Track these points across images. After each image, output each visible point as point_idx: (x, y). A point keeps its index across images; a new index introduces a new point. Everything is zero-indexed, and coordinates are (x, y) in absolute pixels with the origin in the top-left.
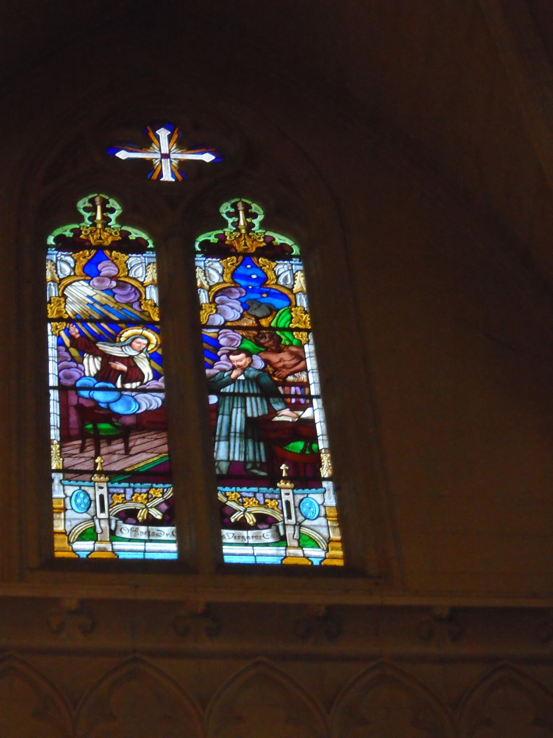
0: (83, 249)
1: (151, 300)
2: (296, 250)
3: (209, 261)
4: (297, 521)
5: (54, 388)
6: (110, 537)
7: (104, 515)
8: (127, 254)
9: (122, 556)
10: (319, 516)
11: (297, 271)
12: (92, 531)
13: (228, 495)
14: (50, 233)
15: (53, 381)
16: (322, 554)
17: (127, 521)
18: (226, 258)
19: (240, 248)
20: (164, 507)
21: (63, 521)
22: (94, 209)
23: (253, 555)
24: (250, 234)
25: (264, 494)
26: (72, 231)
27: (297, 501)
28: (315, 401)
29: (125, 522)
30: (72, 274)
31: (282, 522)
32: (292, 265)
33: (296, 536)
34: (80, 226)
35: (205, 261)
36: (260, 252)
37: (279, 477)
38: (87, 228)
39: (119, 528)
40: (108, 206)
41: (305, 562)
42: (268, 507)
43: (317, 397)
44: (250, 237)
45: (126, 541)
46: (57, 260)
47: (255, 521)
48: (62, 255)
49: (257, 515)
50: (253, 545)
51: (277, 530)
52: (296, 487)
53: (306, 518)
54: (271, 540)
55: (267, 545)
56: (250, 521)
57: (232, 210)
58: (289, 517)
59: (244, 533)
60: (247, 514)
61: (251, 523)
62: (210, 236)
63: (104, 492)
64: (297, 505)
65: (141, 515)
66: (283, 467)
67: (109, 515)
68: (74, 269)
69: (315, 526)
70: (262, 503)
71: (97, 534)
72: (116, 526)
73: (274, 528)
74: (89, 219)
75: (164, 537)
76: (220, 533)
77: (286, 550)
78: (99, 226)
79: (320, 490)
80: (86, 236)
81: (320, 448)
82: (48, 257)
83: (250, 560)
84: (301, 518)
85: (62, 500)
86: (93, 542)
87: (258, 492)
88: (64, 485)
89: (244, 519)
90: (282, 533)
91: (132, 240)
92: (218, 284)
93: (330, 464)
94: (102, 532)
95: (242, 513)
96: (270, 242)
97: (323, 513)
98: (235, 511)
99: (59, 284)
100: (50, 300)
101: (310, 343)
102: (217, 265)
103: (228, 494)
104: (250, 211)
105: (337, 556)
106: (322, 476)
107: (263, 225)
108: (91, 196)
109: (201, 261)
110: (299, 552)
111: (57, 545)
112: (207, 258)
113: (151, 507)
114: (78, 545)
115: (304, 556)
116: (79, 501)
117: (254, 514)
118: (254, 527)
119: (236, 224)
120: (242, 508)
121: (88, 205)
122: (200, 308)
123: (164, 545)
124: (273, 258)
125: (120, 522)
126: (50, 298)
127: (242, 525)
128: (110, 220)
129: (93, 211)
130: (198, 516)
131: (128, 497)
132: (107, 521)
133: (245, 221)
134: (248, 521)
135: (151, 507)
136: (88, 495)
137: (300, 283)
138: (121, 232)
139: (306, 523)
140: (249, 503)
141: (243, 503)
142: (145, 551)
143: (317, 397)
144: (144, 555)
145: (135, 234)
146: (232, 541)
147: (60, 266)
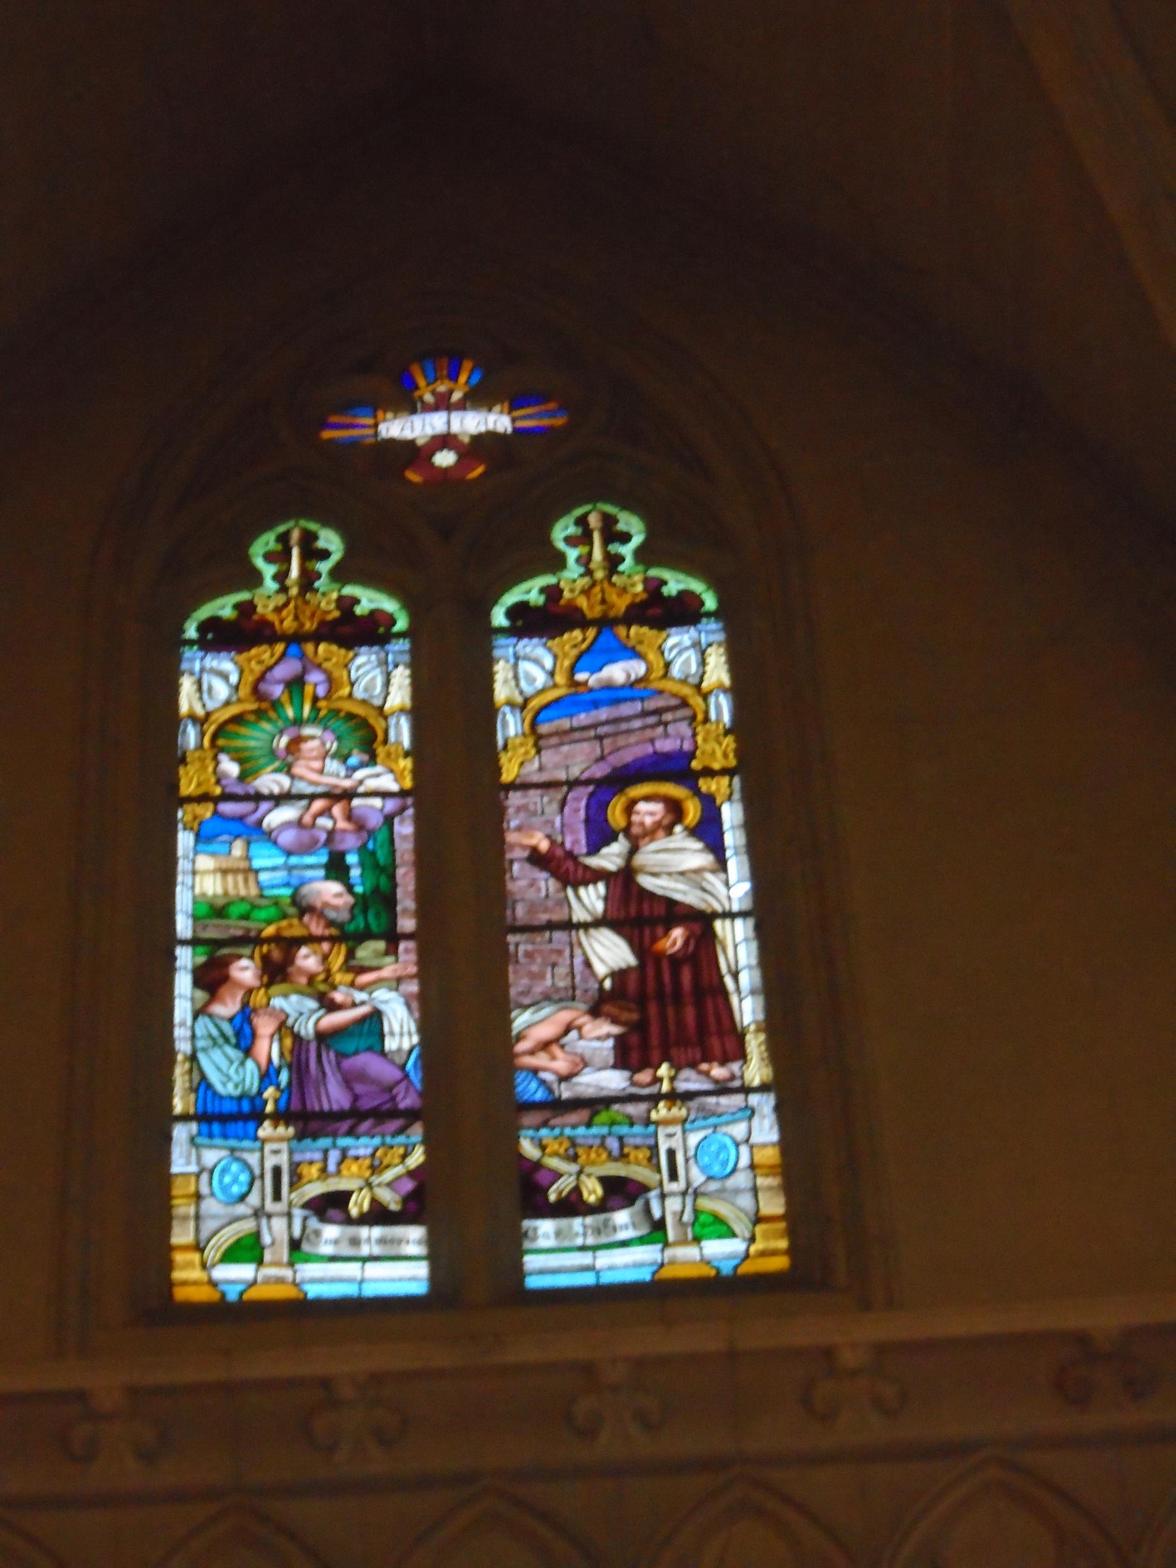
0: (571, 627)
6: (291, 1255)
7: (281, 1207)
9: (313, 1291)
10: (734, 1170)
11: (710, 645)
25: (621, 1139)
26: (542, 590)
30: (234, 698)
32: (700, 632)
49: (605, 1181)
51: (647, 1210)
52: (300, 1136)
55: (624, 1244)
56: (590, 1194)
58: (673, 1176)
59: (577, 1223)
61: (592, 1199)
62: (223, 607)
63: (283, 1160)
65: (358, 1204)
68: (552, 674)
70: (616, 1152)
71: (263, 1249)
72: (304, 1228)
73: (639, 1203)
75: (622, 1235)
77: (663, 1250)
83: (350, 1290)
85: (193, 1179)
86: (659, 1246)
87: (610, 1134)
89: (577, 1190)
90: (657, 1213)
91: (670, 597)
94: (273, 1243)
95: (572, 1178)
96: (654, 587)
97: (744, 1161)
98: (557, 1175)
105: (772, 1252)
107: (641, 555)
108: (281, 529)
113: (379, 1185)
114: (223, 1272)
115: (702, 1260)
116: (227, 1179)
118: (603, 1207)
121: (572, 530)
123: (398, 1268)
125: (314, 1223)
127: (571, 1206)
128: (319, 576)
129: (584, 544)
131: (332, 1167)
135: (379, 1185)
137: (718, 671)
141: (575, 1158)
142: (362, 1282)
145: (675, 583)
146: (550, 1243)
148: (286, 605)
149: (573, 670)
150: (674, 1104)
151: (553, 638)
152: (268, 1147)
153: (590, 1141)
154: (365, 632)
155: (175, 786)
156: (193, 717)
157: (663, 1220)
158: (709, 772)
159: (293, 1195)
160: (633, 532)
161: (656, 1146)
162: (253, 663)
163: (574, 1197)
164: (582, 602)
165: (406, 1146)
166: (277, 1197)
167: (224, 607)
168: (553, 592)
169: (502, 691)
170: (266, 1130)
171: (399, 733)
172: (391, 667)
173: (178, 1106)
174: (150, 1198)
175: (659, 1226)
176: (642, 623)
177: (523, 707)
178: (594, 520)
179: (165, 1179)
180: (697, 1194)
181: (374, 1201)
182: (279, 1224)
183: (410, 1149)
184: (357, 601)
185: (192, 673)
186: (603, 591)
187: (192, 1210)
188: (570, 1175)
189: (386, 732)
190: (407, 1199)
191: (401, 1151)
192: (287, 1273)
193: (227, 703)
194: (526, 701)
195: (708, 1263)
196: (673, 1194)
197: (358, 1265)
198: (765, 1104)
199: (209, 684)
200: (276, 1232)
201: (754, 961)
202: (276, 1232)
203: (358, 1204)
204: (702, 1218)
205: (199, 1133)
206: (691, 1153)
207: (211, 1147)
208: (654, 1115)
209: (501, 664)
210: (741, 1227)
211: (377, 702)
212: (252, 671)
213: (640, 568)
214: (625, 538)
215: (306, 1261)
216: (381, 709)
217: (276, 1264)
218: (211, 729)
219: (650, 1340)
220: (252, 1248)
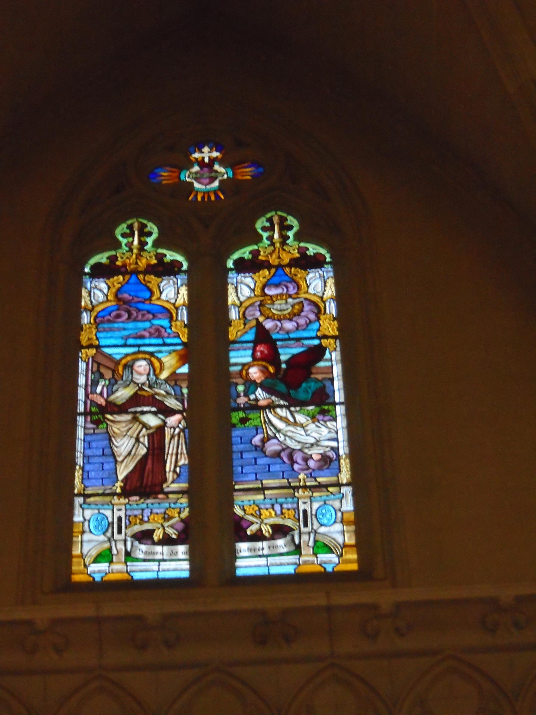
4: (312, 529)
5: (81, 414)
7: (123, 537)
8: (305, 269)
9: (137, 576)
10: (335, 522)
11: (328, 278)
12: (108, 552)
16: (336, 560)
17: (142, 541)
19: (273, 260)
22: (272, 228)
23: (159, 570)
24: (285, 247)
25: (281, 505)
26: (251, 252)
28: (338, 407)
29: (140, 543)
33: (311, 543)
40: (146, 230)
42: (285, 517)
45: (141, 562)
48: (242, 277)
50: (267, 556)
53: (321, 525)
54: (285, 550)
55: (281, 554)
57: (268, 224)
58: (306, 525)
59: (259, 544)
61: (267, 534)
62: (244, 253)
63: (122, 514)
64: (314, 513)
65: (158, 535)
70: (279, 512)
71: (112, 555)
73: (289, 538)
74: (268, 239)
78: (278, 245)
81: (340, 454)
83: (263, 571)
84: (316, 525)
85: (81, 524)
88: (83, 509)
89: (260, 530)
90: (297, 542)
94: (118, 552)
96: (303, 251)
102: (249, 281)
105: (351, 562)
108: (129, 222)
111: (74, 568)
118: (272, 538)
119: (130, 245)
122: (229, 323)
123: (175, 564)
125: (136, 543)
127: (258, 537)
128: (288, 237)
131: (146, 519)
132: (123, 543)
138: (299, 248)
139: (322, 530)
143: (340, 404)
145: (312, 249)
146: (247, 554)
147: (94, 293)
148: (274, 251)
149: (263, 289)
150: (121, 497)
151: (254, 273)
154: (169, 269)
155: (79, 341)
156: (234, 305)
159: (127, 531)
162: (261, 279)
163: (259, 533)
165: (180, 509)
166: (120, 532)
167: (102, 258)
169: (232, 298)
174: (64, 533)
176: (150, 274)
177: (91, 310)
178: (276, 220)
179: (70, 523)
181: (165, 534)
183: (182, 509)
189: (325, 308)
190: (180, 534)
194: (93, 307)
196: (120, 540)
197: (265, 559)
198: (347, 491)
199: (98, 292)
203: (158, 535)
204: (318, 544)
206: (314, 513)
207: (88, 509)
208: (113, 502)
211: (173, 301)
213: (153, 249)
214: (290, 228)
215: (133, 561)
216: (322, 298)
217: (119, 562)
218: (94, 314)
219: (112, 609)
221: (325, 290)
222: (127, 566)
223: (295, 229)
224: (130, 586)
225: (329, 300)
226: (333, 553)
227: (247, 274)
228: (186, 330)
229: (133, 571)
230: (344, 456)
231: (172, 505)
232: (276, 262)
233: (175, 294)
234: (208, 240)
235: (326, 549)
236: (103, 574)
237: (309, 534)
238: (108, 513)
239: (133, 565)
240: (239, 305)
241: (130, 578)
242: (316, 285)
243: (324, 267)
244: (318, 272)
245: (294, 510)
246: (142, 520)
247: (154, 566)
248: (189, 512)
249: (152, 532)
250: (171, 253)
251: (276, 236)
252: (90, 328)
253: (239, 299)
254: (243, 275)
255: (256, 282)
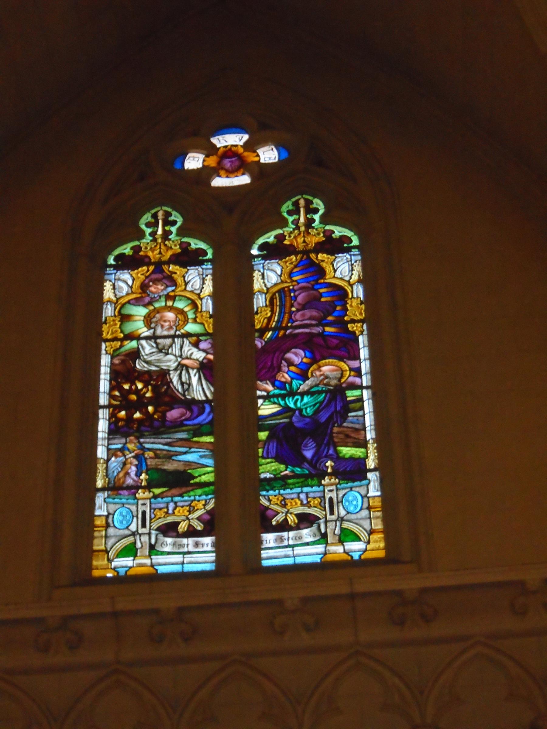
1: (358, 297)
2: (355, 241)
3: (268, 263)
4: (339, 517)
5: (103, 407)
9: (162, 569)
10: (361, 509)
11: (356, 262)
12: (132, 546)
13: (269, 499)
14: (110, 253)
15: (103, 400)
18: (138, 269)
19: (154, 256)
20: (207, 517)
21: (372, 516)
22: (156, 224)
25: (307, 494)
26: (132, 248)
27: (340, 495)
29: (165, 536)
31: (324, 519)
33: (337, 531)
34: (284, 231)
35: (263, 264)
36: (320, 248)
37: (323, 474)
38: (148, 243)
39: (160, 542)
41: (346, 557)
42: (311, 506)
43: (367, 388)
44: (165, 245)
46: (115, 279)
47: (296, 521)
50: (293, 546)
51: (319, 528)
53: (348, 513)
54: (310, 539)
55: (307, 544)
58: (332, 513)
60: (289, 515)
62: (269, 238)
65: (183, 527)
66: (329, 463)
67: (150, 529)
69: (357, 519)
70: (305, 502)
71: (137, 549)
73: (315, 526)
74: (150, 234)
75: (205, 549)
76: (260, 537)
78: (160, 240)
79: (364, 482)
80: (289, 241)
81: (368, 439)
82: (106, 277)
83: (289, 561)
87: (302, 492)
89: (286, 520)
90: (323, 531)
92: (276, 285)
93: (376, 454)
94: (142, 546)
96: (328, 235)
97: (366, 505)
99: (115, 304)
100: (106, 320)
101: (364, 333)
103: (271, 497)
104: (311, 207)
105: (377, 547)
106: (368, 468)
108: (153, 211)
109: (112, 274)
110: (340, 549)
112: (266, 260)
113: (192, 519)
114: (118, 562)
117: (296, 515)
118: (298, 527)
119: (296, 222)
120: (284, 510)
121: (150, 219)
123: (200, 556)
124: (184, 265)
125: (161, 537)
126: (106, 318)
127: (284, 527)
128: (170, 233)
130: (238, 521)
133: (164, 230)
134: (290, 523)
136: (132, 512)
140: (291, 505)
141: (284, 506)
142: (183, 563)
144: (183, 567)
145: (338, 231)
146: (272, 544)
151: (133, 270)
152: (140, 502)
153: (292, 496)
156: (110, 301)
157: (326, 532)
158: (353, 321)
160: (178, 220)
161: (324, 497)
164: (150, 254)
166: (144, 526)
168: (137, 249)
170: (326, 481)
171: (207, 306)
172: (204, 276)
173: (100, 483)
175: (324, 536)
178: (302, 202)
180: (342, 520)
181: (190, 526)
182: (145, 538)
183: (208, 501)
184: (334, 232)
185: (110, 281)
186: (160, 248)
187: (103, 533)
188: (283, 513)
191: (203, 502)
192: (148, 561)
193: (127, 294)
195: (347, 553)
196: (144, 534)
199: (119, 285)
200: (142, 542)
201: (371, 410)
202: (142, 542)
203: (183, 527)
205: (108, 497)
209: (257, 272)
210: (364, 536)
211: (347, 278)
212: (139, 278)
214: (316, 211)
215: (157, 555)
216: (199, 295)
220: (131, 550)
221: (203, 288)
222: (151, 559)
223: (321, 212)
224: (153, 579)
225: (206, 298)
226: (360, 540)
227: (126, 271)
228: (211, 320)
229: (159, 564)
230: (371, 442)
231: (197, 498)
232: (301, 247)
233: (349, 271)
234: (228, 227)
235: (352, 537)
236: (127, 569)
237: (336, 521)
238: (134, 508)
239: (157, 559)
240: (265, 291)
241: (154, 571)
242: (341, 271)
243: (351, 251)
244: (345, 256)
245: (320, 497)
246: (167, 513)
247: (178, 558)
248: (215, 503)
249: (177, 524)
250: (197, 241)
251: (304, 221)
252: (114, 321)
253: (265, 285)
254: (121, 272)
255: (283, 268)
